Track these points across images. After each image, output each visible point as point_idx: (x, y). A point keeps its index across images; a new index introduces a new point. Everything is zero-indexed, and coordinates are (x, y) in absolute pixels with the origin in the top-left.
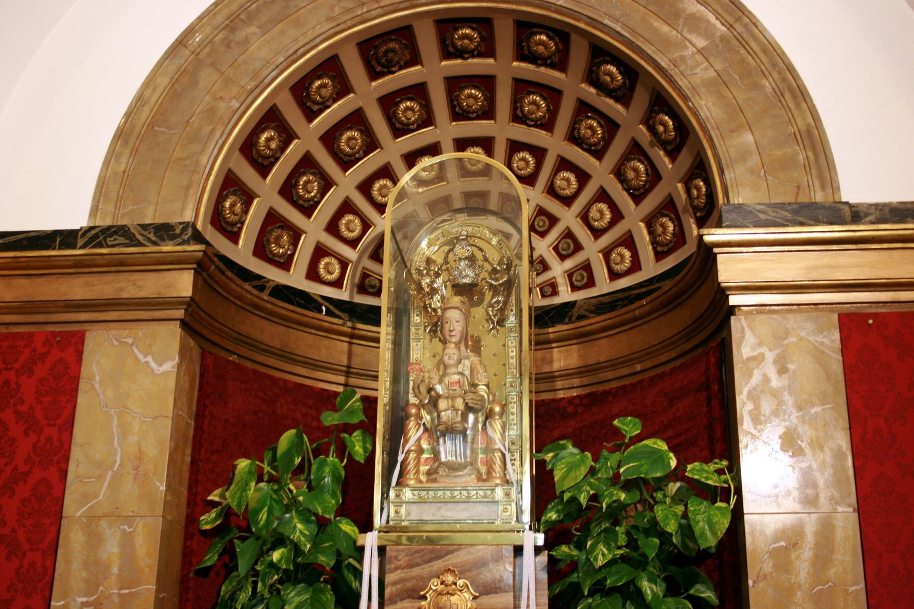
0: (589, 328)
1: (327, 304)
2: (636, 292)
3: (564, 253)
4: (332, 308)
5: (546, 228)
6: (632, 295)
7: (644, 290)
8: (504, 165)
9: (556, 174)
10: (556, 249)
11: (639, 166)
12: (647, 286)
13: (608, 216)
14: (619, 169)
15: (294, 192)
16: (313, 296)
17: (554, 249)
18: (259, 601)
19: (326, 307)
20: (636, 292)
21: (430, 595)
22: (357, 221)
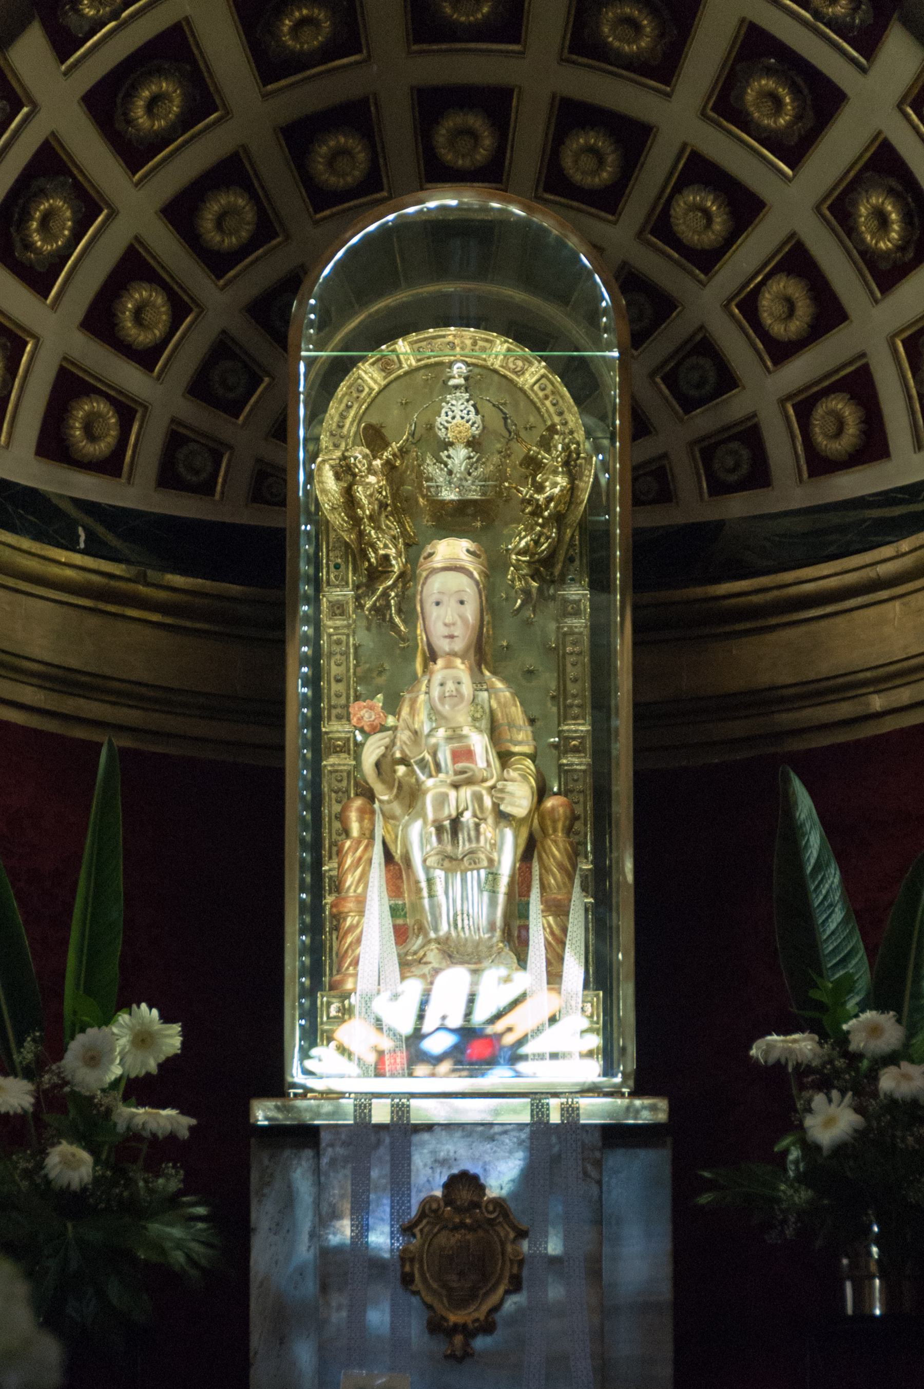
0: (755, 599)
1: (89, 521)
2: (876, 513)
3: (694, 393)
4: (100, 530)
5: (733, 478)
6: (864, 521)
7: (897, 511)
8: (617, 279)
9: (678, 189)
10: (671, 380)
11: (890, 213)
12: (901, 502)
13: (804, 310)
14: (841, 198)
15: (16, 238)
16: (55, 501)
17: (702, 451)
18: (355, 1194)
19: (85, 529)
20: (876, 513)
21: (421, 1230)
22: (159, 299)
